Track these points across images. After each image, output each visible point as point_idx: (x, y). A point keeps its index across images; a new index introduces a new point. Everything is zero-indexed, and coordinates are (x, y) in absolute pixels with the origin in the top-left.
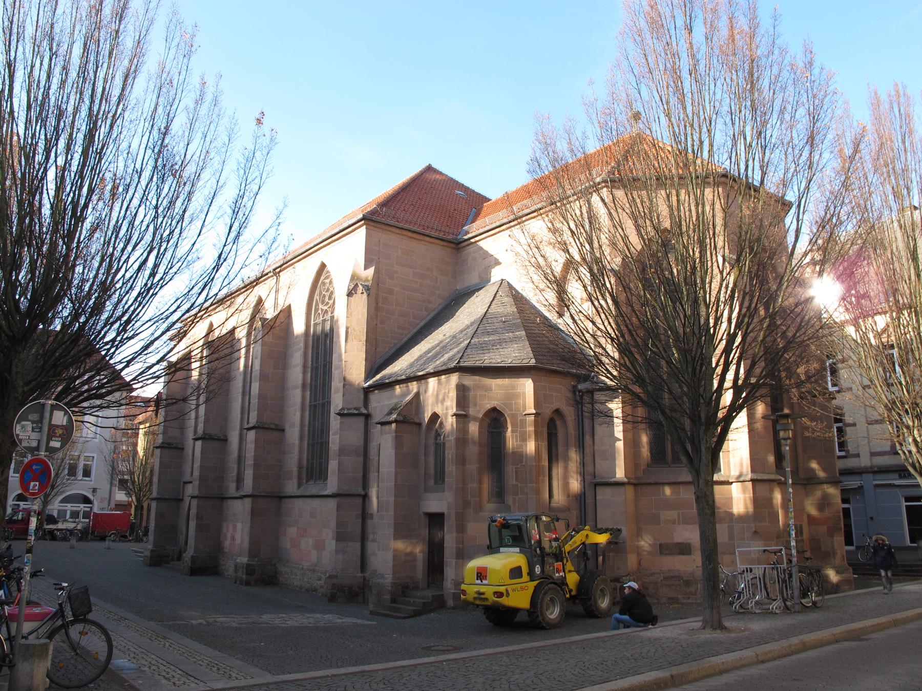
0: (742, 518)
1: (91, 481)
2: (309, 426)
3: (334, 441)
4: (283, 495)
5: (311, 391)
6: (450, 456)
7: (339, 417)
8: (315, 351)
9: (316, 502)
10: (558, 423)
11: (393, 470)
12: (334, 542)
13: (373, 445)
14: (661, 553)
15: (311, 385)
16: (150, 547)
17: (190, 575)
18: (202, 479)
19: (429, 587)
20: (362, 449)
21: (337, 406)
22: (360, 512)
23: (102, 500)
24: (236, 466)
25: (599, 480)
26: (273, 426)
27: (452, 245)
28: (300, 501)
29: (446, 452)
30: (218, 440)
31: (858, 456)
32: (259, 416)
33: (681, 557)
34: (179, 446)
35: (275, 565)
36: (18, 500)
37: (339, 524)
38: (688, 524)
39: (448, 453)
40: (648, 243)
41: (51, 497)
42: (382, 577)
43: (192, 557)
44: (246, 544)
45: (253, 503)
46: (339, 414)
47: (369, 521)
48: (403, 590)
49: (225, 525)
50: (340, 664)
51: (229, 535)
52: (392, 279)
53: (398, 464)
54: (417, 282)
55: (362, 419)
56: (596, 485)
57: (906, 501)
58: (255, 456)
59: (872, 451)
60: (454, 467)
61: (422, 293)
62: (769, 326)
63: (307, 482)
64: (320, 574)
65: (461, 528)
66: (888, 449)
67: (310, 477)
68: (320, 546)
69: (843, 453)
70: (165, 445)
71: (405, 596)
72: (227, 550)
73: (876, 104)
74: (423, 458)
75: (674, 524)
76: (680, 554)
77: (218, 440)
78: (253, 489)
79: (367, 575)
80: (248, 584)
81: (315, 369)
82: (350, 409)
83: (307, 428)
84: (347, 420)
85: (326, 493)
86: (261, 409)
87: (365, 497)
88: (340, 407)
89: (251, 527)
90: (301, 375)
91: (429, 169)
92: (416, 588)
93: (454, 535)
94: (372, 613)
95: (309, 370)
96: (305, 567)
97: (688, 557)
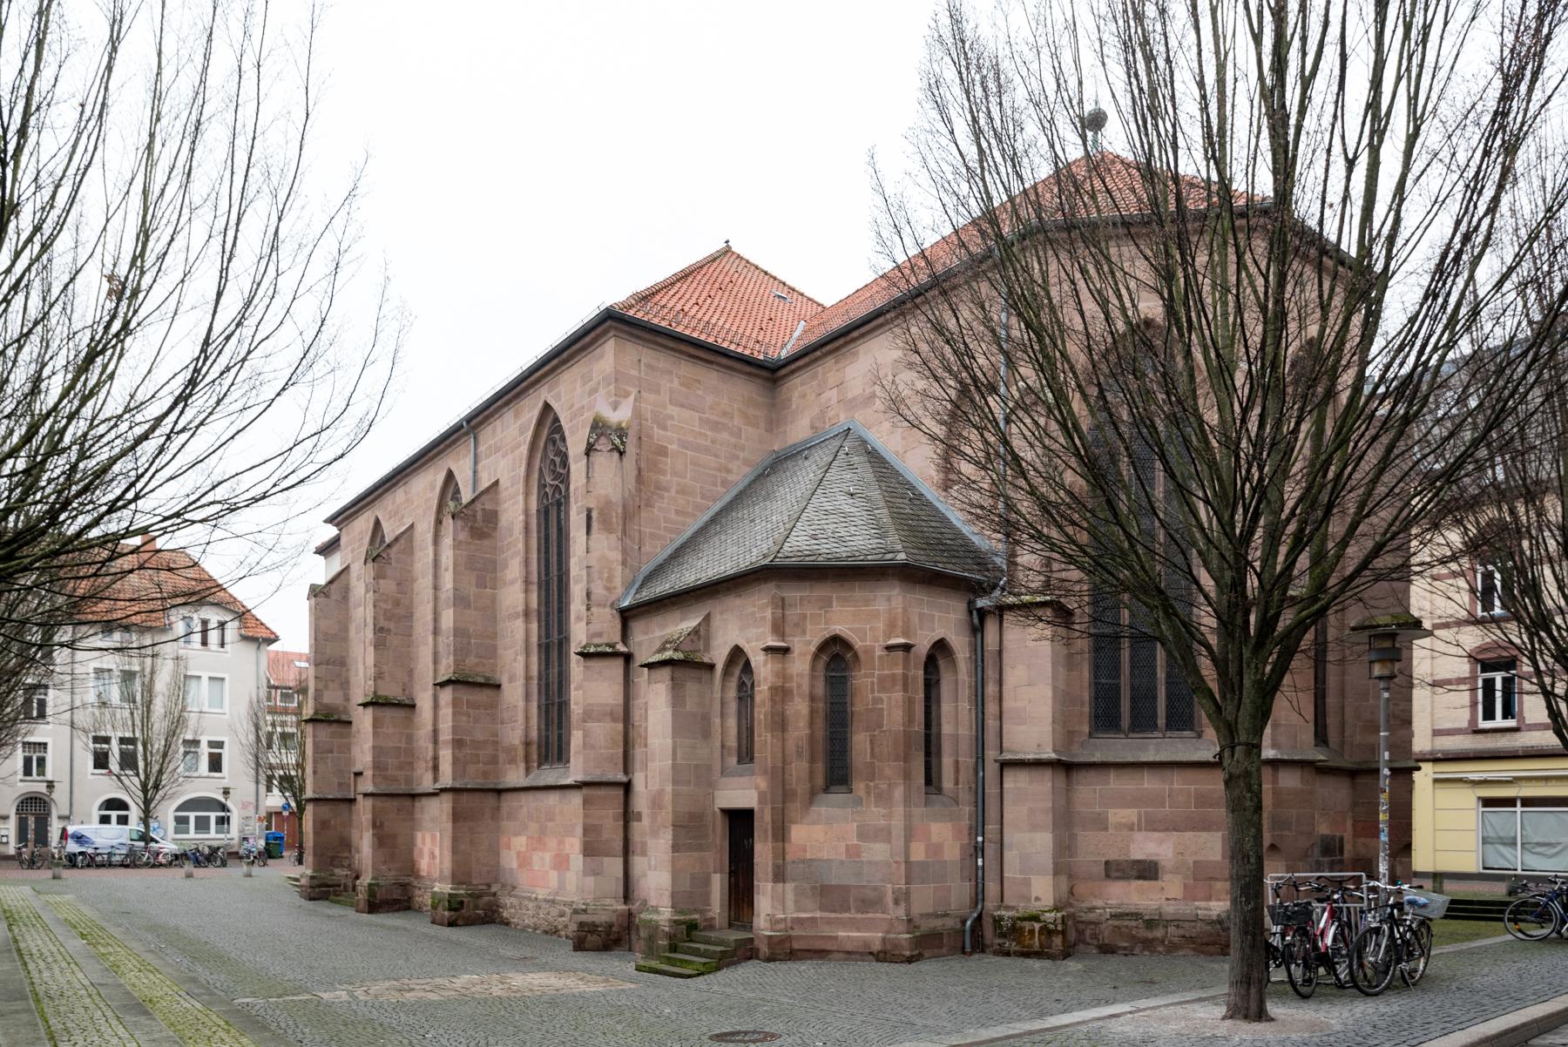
2: (540, 679)
4: (501, 787)
5: (539, 622)
6: (762, 717)
8: (543, 555)
9: (552, 799)
11: (669, 741)
13: (637, 704)
15: (539, 611)
17: (369, 912)
18: (378, 766)
19: (730, 925)
20: (621, 710)
22: (621, 811)
23: (245, 806)
25: (1007, 756)
26: (481, 680)
27: (764, 373)
28: (530, 796)
30: (399, 705)
34: (344, 717)
35: (495, 894)
36: (107, 809)
37: (586, 830)
38: (1155, 830)
39: (759, 713)
40: (1063, 175)
41: (155, 802)
42: (656, 910)
43: (370, 885)
45: (455, 801)
46: (580, 654)
47: (635, 825)
48: (687, 932)
49: (419, 835)
51: (426, 852)
52: (664, 428)
53: (677, 731)
54: (706, 436)
55: (620, 663)
56: (1004, 765)
58: (453, 727)
59: (1436, 727)
63: (539, 765)
64: (562, 907)
65: (781, 834)
66: (1465, 724)
68: (561, 863)
70: (320, 717)
71: (691, 941)
72: (423, 873)
74: (717, 721)
75: (1132, 830)
76: (1139, 878)
77: (399, 705)
79: (635, 907)
80: (452, 924)
81: (544, 586)
83: (536, 682)
84: (596, 664)
85: (569, 781)
86: (460, 652)
87: (627, 787)
88: (584, 643)
90: (522, 595)
91: (727, 251)
92: (711, 927)
93: (770, 845)
95: (535, 588)
96: (540, 897)
97: (1152, 883)
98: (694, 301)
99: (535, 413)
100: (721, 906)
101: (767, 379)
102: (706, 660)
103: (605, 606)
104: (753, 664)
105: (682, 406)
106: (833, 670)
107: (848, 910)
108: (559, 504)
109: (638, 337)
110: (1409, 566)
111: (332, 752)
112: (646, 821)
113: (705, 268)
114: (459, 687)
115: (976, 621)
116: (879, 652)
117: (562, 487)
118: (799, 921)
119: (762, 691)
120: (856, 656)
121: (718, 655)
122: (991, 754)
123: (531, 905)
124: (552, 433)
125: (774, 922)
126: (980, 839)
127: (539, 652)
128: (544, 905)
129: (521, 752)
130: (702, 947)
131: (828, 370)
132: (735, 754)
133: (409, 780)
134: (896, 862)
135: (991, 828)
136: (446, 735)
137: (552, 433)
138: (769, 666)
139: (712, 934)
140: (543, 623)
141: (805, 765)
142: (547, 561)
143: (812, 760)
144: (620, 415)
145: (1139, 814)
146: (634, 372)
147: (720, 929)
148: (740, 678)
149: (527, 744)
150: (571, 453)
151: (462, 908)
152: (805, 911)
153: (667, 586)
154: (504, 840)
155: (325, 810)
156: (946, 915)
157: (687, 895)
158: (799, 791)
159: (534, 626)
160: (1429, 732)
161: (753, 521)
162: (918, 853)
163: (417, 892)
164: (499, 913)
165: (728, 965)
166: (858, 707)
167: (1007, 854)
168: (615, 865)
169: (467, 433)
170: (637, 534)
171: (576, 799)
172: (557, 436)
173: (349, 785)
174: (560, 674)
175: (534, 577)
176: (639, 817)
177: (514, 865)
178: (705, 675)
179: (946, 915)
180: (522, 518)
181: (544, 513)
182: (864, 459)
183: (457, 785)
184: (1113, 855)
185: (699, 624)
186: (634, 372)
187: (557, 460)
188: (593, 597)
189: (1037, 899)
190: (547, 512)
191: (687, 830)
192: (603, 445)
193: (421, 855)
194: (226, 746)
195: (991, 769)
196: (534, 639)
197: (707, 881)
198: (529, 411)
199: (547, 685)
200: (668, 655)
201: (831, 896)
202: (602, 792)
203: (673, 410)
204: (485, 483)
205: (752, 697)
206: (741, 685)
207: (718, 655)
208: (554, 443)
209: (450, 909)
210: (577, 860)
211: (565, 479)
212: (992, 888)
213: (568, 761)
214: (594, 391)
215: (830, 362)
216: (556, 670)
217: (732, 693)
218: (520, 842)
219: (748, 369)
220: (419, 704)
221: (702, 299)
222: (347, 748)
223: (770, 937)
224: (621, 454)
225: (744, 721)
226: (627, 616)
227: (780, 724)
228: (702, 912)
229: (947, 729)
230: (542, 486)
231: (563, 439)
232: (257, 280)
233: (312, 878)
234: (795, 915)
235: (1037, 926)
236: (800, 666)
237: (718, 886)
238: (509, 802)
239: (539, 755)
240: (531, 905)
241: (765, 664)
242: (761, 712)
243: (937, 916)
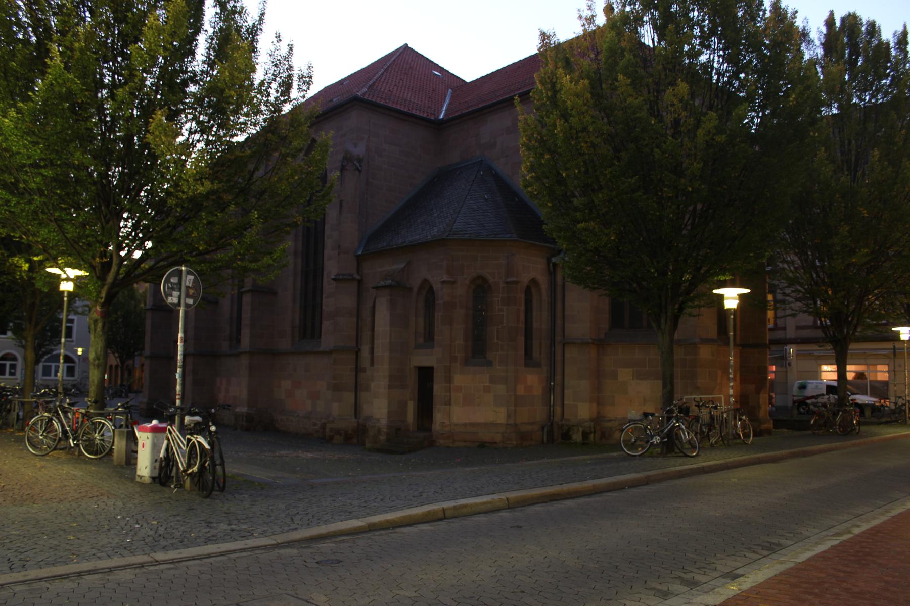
0: (217, 428)
1: (73, 341)
7: (375, 290)
10: (533, 290)
57: (50, 375)
65: (449, 379)
66: (811, 323)
73: (830, 22)
85: (320, 350)
91: (406, 45)
98: (394, 84)
110: (767, 306)
115: (552, 269)
122: (558, 338)
126: (552, 384)
135: (558, 378)
144: (359, 150)
159: (299, 260)
162: (521, 390)
167: (566, 392)
168: (349, 397)
185: (405, 267)
191: (396, 380)
194: (76, 322)
212: (558, 409)
221: (398, 81)
224: (360, 171)
226: (360, 259)
229: (535, 325)
237: (411, 407)
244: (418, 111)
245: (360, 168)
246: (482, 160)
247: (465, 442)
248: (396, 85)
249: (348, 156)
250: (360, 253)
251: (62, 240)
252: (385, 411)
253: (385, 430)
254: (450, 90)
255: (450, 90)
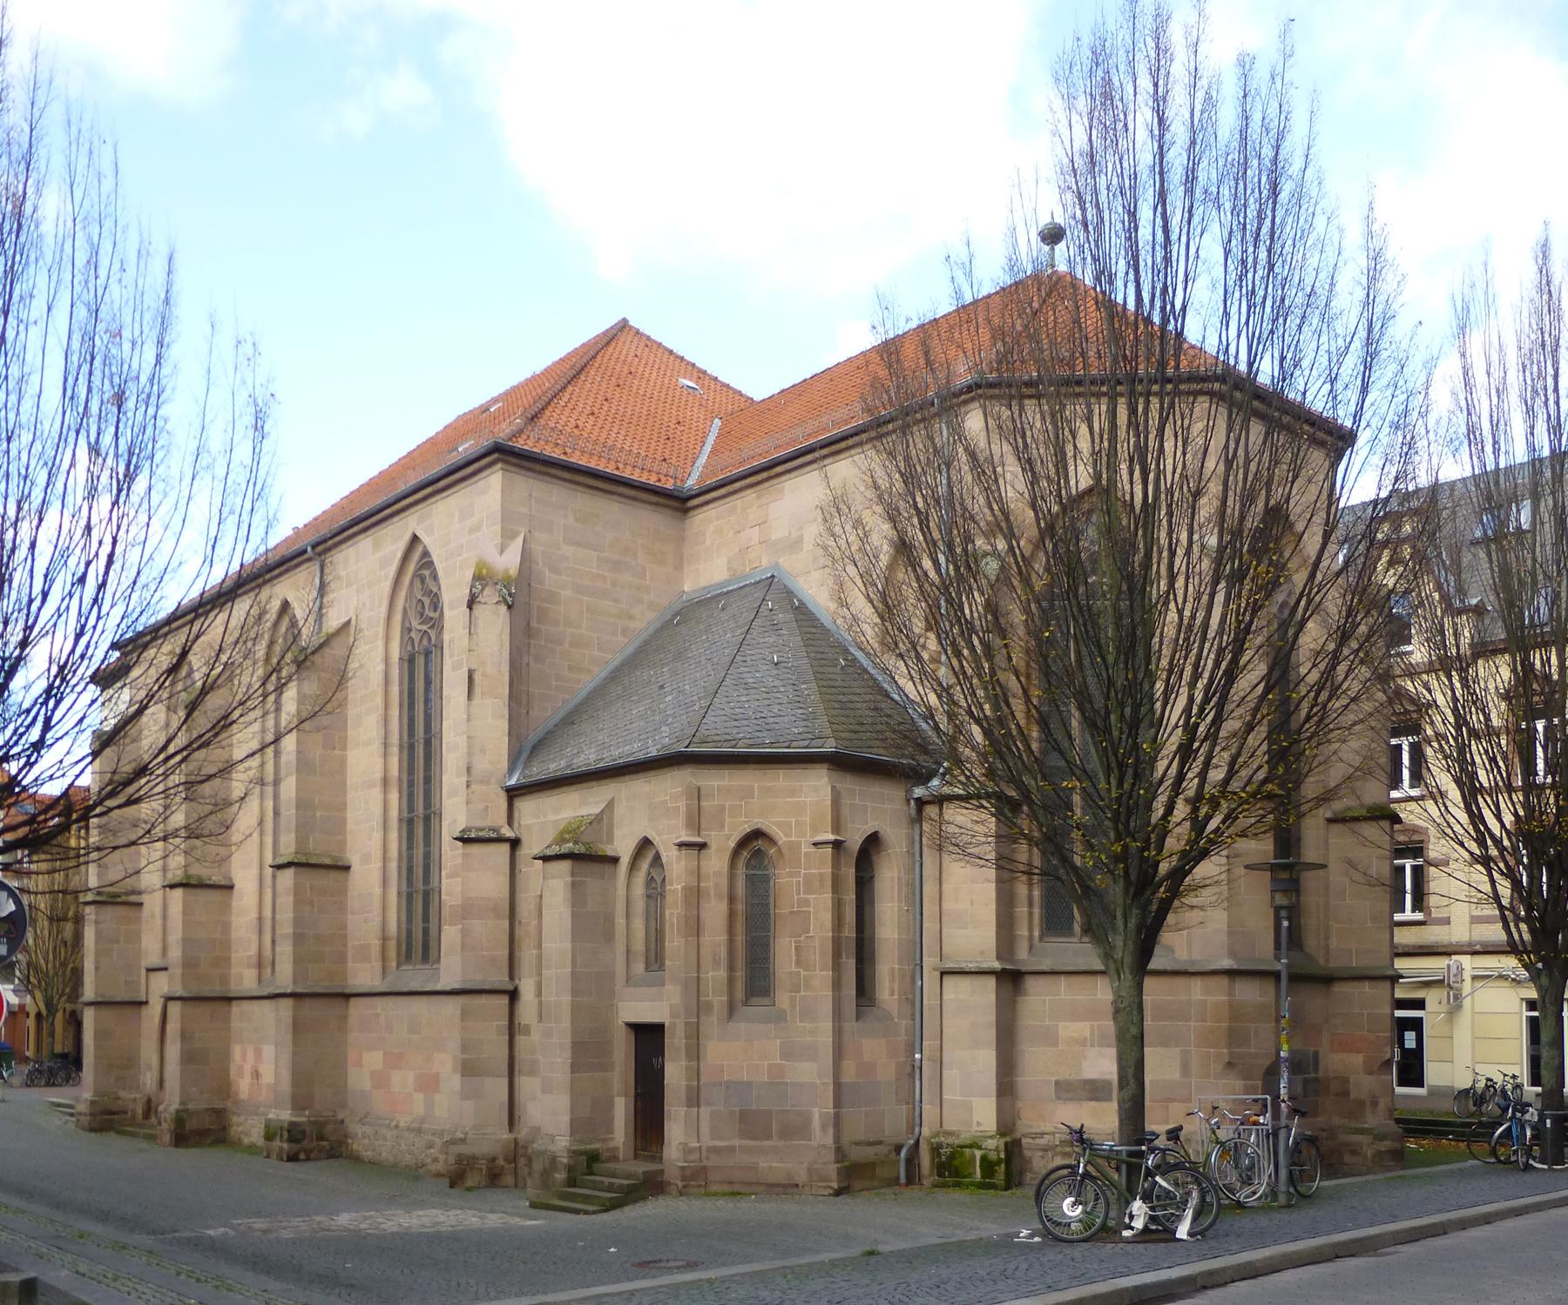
3: (451, 889)
5: (400, 793)
11: (568, 945)
12: (457, 1078)
14: (1058, 1097)
15: (400, 780)
16: (87, 1095)
19: (636, 1157)
21: (454, 821)
24: (255, 937)
25: (949, 965)
26: (327, 861)
29: (667, 912)
31: (1447, 921)
32: (301, 840)
33: (1093, 1104)
37: (465, 1047)
39: (671, 914)
43: (178, 1111)
44: (286, 1086)
47: (521, 1040)
48: (589, 1162)
49: (237, 1052)
50: (492, 1295)
51: (248, 1068)
55: (506, 847)
58: (295, 918)
60: (683, 940)
61: (616, 600)
62: (1110, 734)
64: (430, 1137)
65: (695, 1052)
67: (406, 956)
68: (429, 1084)
69: (1419, 916)
75: (1084, 1045)
76: (1091, 1099)
78: (295, 982)
80: (292, 1158)
82: (481, 830)
85: (439, 987)
86: (304, 828)
87: (513, 995)
89: (295, 1054)
91: (624, 325)
92: (615, 1158)
94: (534, 1205)
96: (402, 1124)
99: (402, 545)
100: (626, 1134)
101: (675, 509)
102: (610, 853)
103: (488, 783)
104: (664, 860)
105: (578, 544)
106: (754, 868)
107: (769, 1137)
108: (427, 654)
109: (528, 469)
111: (118, 942)
112: (536, 1036)
113: (599, 358)
114: (302, 870)
116: (806, 849)
117: (432, 634)
118: (716, 1150)
119: (676, 886)
120: (780, 851)
121: (623, 847)
123: (389, 1134)
124: (420, 569)
125: (687, 1150)
127: (400, 830)
128: (406, 1134)
129: (375, 951)
130: (607, 1180)
131: (747, 503)
132: (643, 959)
133: (224, 979)
134: (823, 1084)
136: (286, 929)
137: (420, 569)
138: (683, 863)
139: (612, 1166)
140: (405, 794)
141: (722, 973)
142: (411, 721)
143: (731, 968)
145: (1092, 1028)
146: (523, 510)
147: (625, 1160)
148: (649, 873)
149: (385, 939)
150: (446, 597)
151: (304, 1138)
152: (723, 1139)
153: (563, 763)
154: (352, 1055)
155: (109, 1015)
156: (880, 1143)
157: (587, 1120)
158: (716, 1004)
159: (394, 797)
160: (1467, 919)
161: (662, 687)
163: (235, 1119)
164: (347, 1145)
165: (635, 1201)
166: (783, 910)
169: (309, 560)
170: (524, 696)
171: (451, 1006)
172: (426, 573)
173: (139, 983)
174: (427, 855)
175: (395, 739)
176: (527, 1030)
177: (367, 1086)
178: (607, 868)
179: (880, 1143)
180: (381, 667)
181: (409, 661)
182: (790, 616)
183: (300, 990)
184: (1065, 1074)
186: (523, 510)
187: (427, 601)
188: (473, 772)
189: (979, 1124)
190: (411, 661)
192: (489, 595)
193: (241, 1074)
195: (930, 979)
196: (394, 813)
197: (610, 1106)
198: (388, 543)
199: (410, 869)
200: (568, 847)
201: (752, 1123)
202: (483, 1001)
203: (568, 550)
204: (333, 621)
205: (662, 895)
206: (650, 880)
207: (623, 847)
208: (423, 580)
209: (290, 1140)
210: (452, 1081)
211: (437, 624)
213: (438, 960)
214: (478, 528)
215: (750, 495)
216: (421, 851)
217: (639, 890)
218: (374, 1060)
219: (654, 499)
220: (238, 884)
222: (135, 937)
223: (683, 1168)
225: (653, 923)
226: (513, 793)
227: (695, 927)
228: (604, 1141)
230: (407, 630)
231: (435, 577)
232: (213, 534)
233: (92, 1103)
234: (712, 1143)
235: (978, 1154)
236: (716, 862)
237: (621, 1110)
238: (357, 1008)
239: (399, 953)
240: (389, 1134)
241: (679, 860)
242: (674, 912)
243: (870, 1144)
244: (638, 471)
245: (509, 600)
246: (773, 576)
247: (731, 1183)
248: (593, 414)
249: (484, 571)
250: (513, 782)
251: (1089, 405)
252: (565, 1119)
253: (565, 1160)
254: (717, 422)
255: (717, 422)
